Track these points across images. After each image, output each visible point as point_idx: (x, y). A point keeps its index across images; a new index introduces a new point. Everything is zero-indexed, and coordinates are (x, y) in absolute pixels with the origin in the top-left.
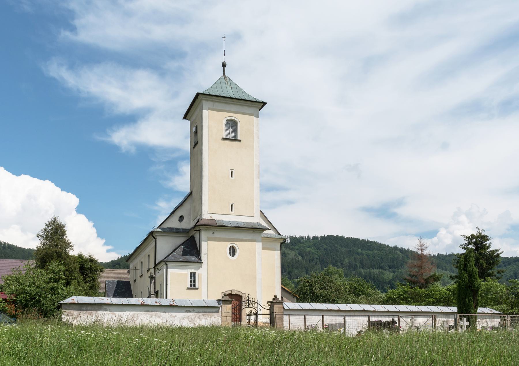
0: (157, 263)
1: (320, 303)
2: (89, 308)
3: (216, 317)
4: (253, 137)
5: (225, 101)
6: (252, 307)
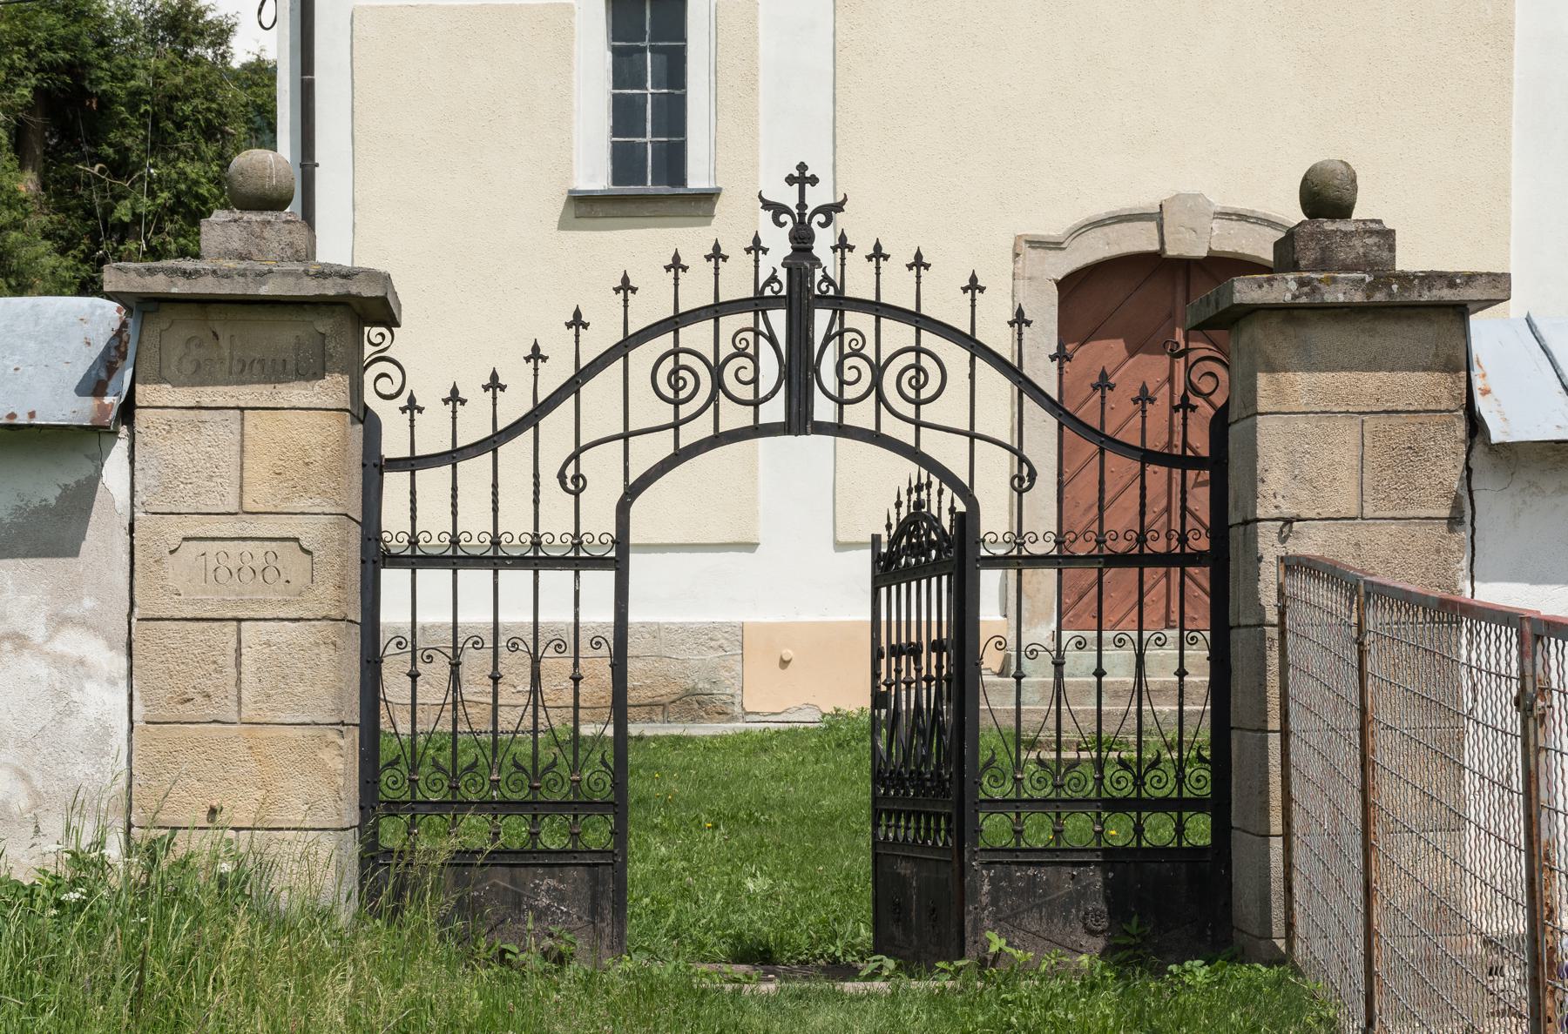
6: (861, 415)
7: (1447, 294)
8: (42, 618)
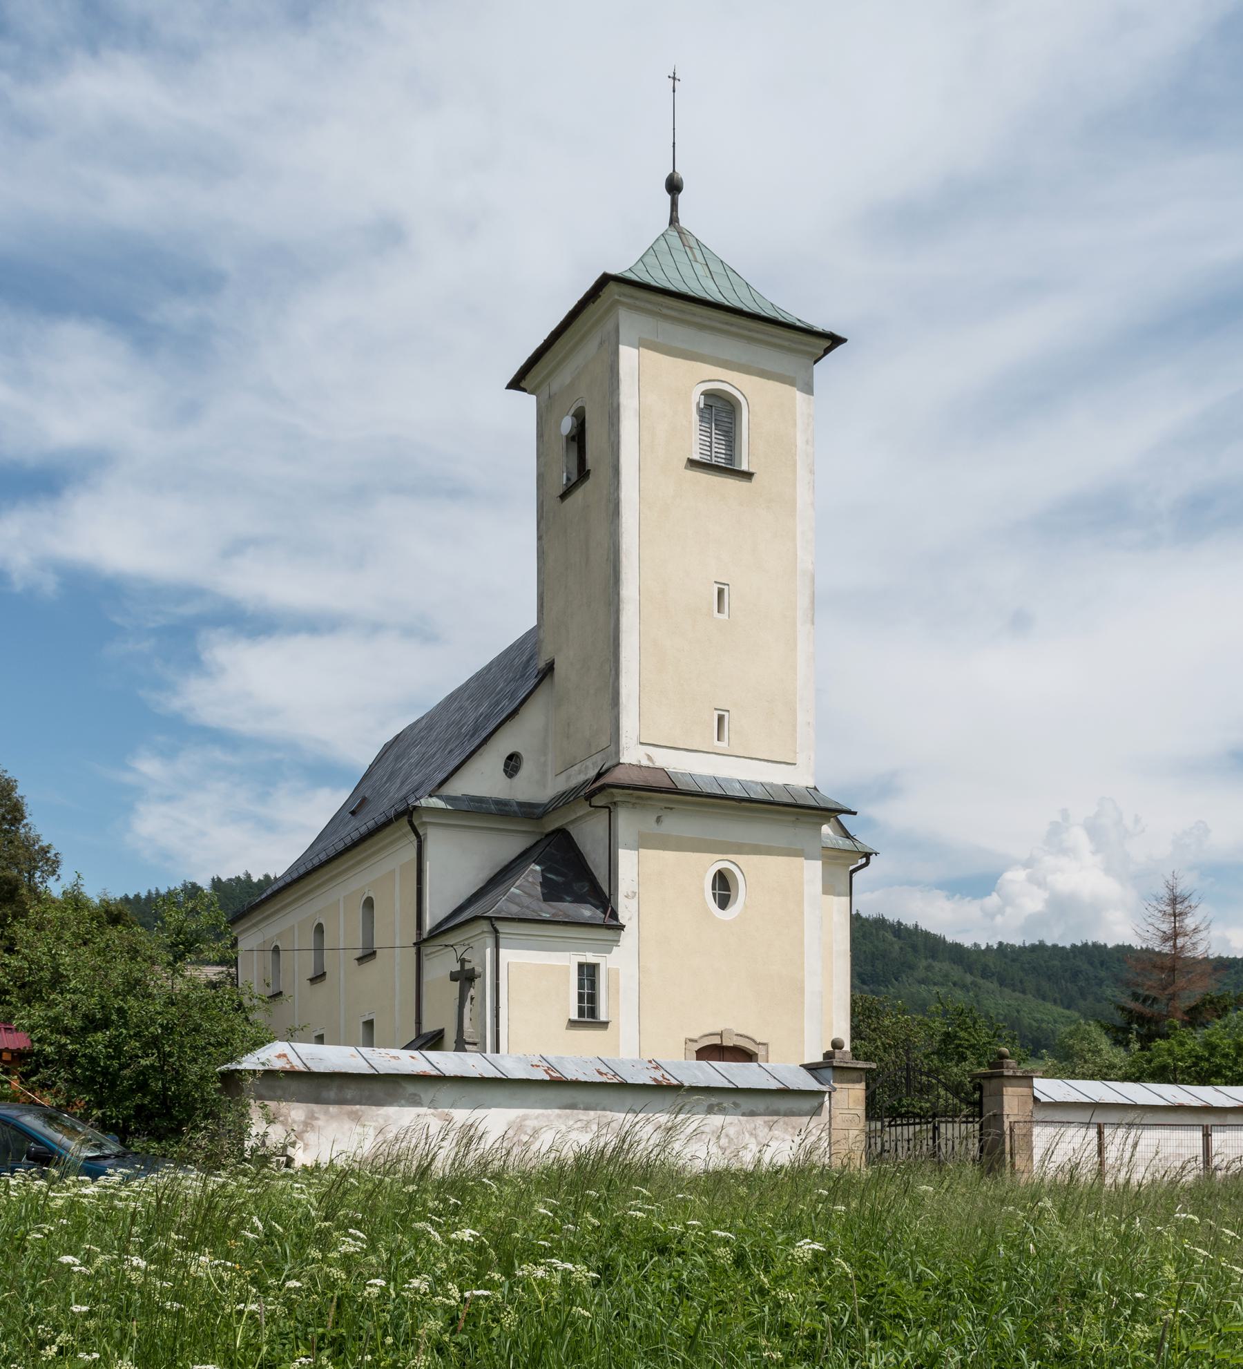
0: (428, 924)
2: (349, 1093)
4: (795, 465)
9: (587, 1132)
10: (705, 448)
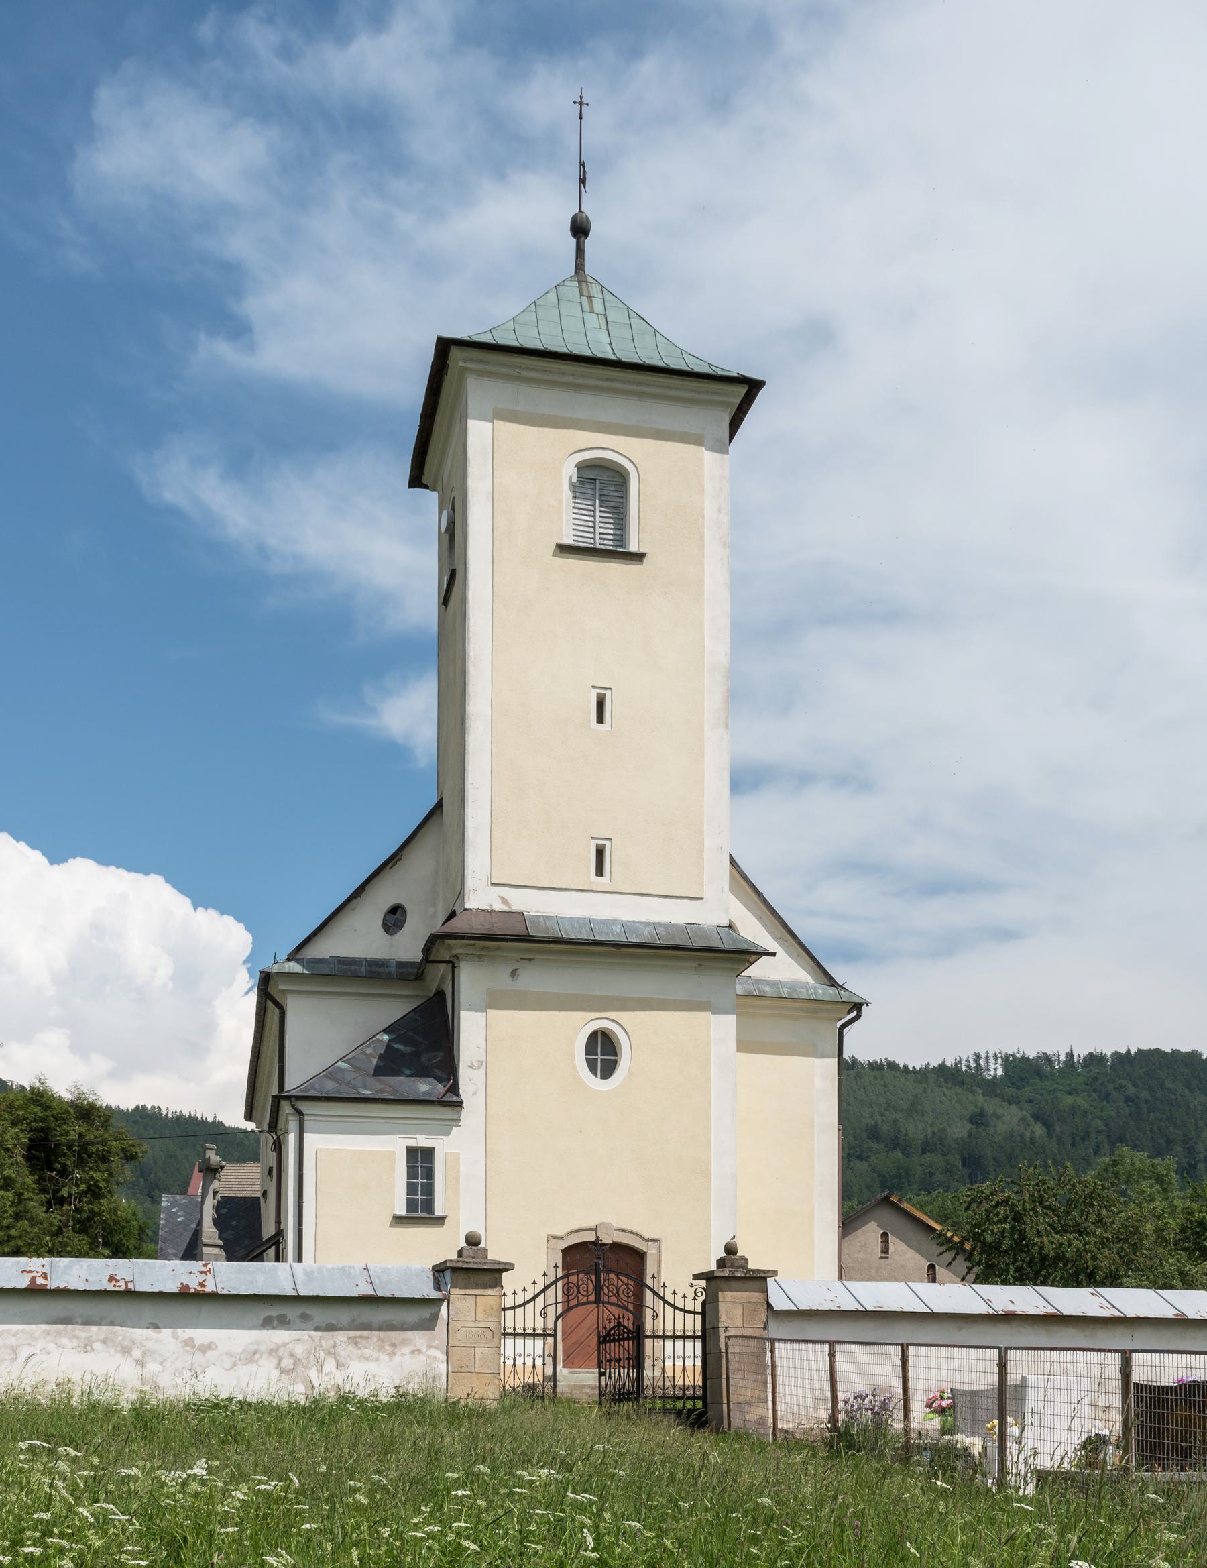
1: (1052, 1285)
3: (419, 1351)
4: (702, 539)
5: (570, 379)
6: (613, 1300)
7: (763, 1275)
8: (425, 1346)
9: (85, 1352)
10: (587, 529)
